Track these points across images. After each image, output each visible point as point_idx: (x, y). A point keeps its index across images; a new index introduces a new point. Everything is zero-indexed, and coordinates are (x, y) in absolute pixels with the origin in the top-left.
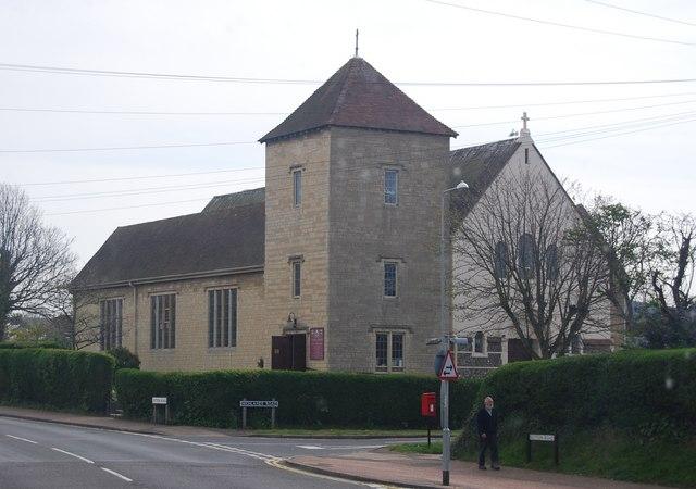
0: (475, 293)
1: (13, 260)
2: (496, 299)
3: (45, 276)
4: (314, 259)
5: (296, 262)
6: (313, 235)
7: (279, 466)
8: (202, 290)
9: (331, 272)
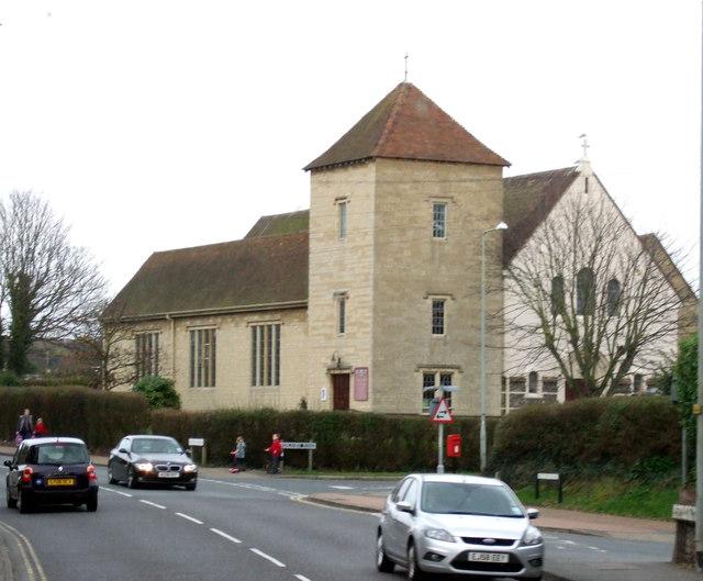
0: (521, 333)
1: (33, 284)
2: (542, 340)
3: (71, 302)
4: (358, 296)
5: (342, 299)
6: (357, 271)
7: (306, 502)
8: (244, 324)
9: (375, 310)
